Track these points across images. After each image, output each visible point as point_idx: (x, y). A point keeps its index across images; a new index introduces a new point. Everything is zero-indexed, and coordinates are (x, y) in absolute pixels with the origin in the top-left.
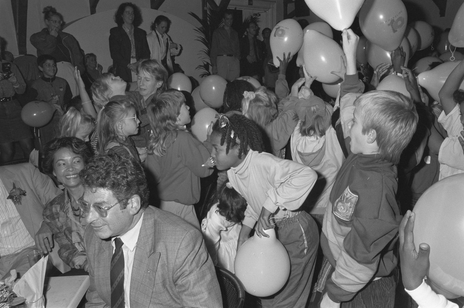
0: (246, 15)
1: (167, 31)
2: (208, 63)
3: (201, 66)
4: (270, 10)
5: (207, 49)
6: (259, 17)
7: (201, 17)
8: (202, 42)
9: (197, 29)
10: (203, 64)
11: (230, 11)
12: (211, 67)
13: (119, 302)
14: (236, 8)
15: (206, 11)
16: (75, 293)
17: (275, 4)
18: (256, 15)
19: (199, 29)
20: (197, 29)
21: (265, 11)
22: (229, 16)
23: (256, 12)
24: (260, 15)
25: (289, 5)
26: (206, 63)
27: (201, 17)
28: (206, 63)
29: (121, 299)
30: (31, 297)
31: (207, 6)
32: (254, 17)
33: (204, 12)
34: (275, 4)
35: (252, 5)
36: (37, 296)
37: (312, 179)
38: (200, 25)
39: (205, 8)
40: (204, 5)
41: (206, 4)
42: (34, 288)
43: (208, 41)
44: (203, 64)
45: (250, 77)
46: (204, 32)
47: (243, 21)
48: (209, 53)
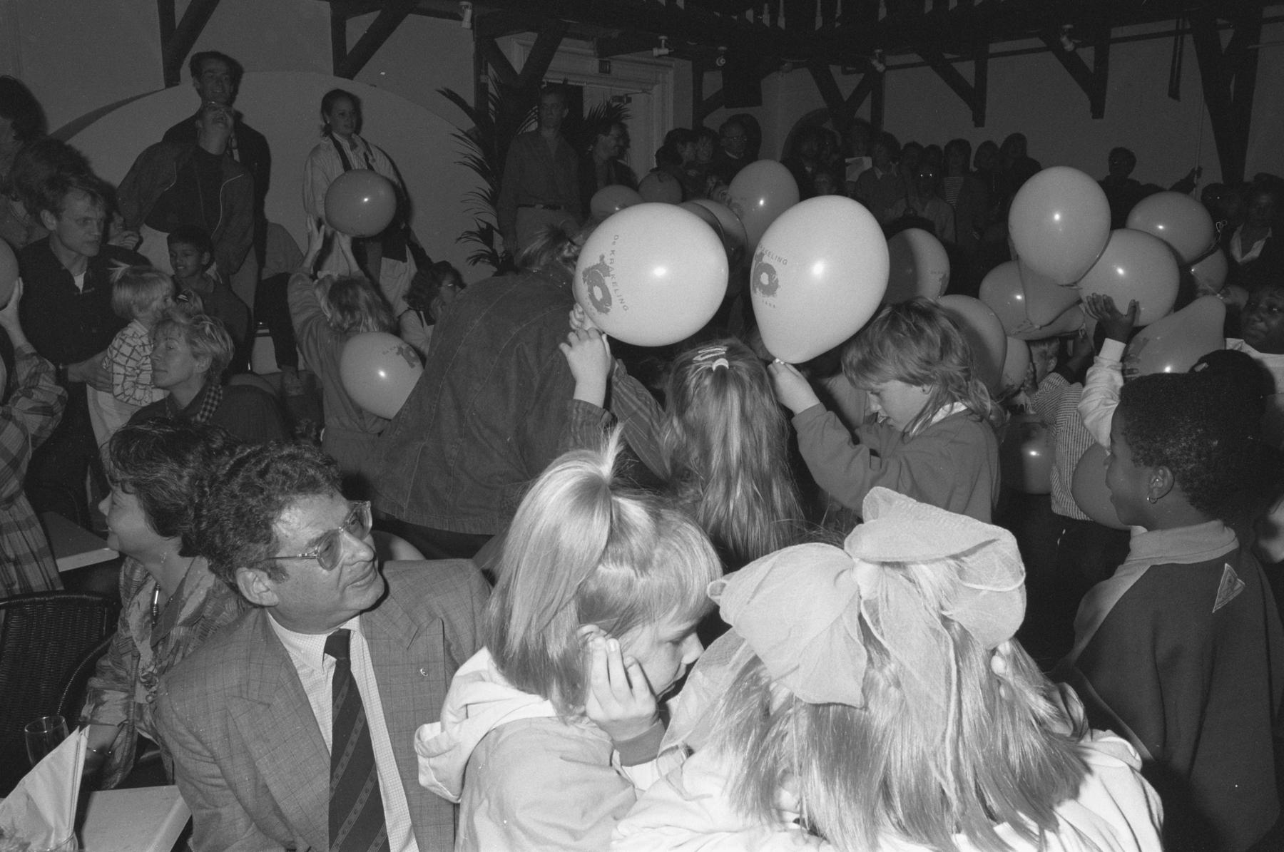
0: (593, 101)
1: (357, 129)
2: (489, 225)
3: (471, 233)
4: (656, 87)
5: (487, 187)
6: (628, 106)
7: (471, 102)
8: (476, 169)
9: (461, 134)
10: (476, 229)
11: (552, 87)
12: (498, 239)
13: (354, 737)
14: (566, 81)
15: (486, 85)
16: (170, 809)
17: (671, 72)
18: (620, 99)
19: (466, 134)
20: (461, 134)
21: (644, 91)
22: (550, 100)
23: (620, 92)
24: (629, 100)
25: (706, 76)
26: (484, 226)
27: (471, 102)
28: (484, 226)
29: (358, 726)
30: (43, 836)
31: (486, 73)
32: (614, 105)
33: (481, 89)
34: (671, 72)
35: (609, 72)
36: (58, 835)
37: (698, 202)
38: (469, 124)
39: (483, 79)
40: (480, 68)
41: (486, 69)
42: (50, 815)
43: (492, 164)
44: (476, 229)
45: (758, 251)
46: (479, 143)
47: (586, 114)
48: (493, 199)
